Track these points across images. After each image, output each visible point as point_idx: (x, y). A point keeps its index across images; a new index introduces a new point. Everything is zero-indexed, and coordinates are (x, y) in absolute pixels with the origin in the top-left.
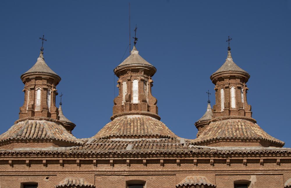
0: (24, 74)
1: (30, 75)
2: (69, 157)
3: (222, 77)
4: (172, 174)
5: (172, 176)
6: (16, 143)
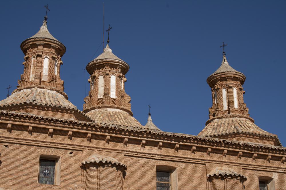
0: (30, 39)
1: (38, 41)
2: (99, 131)
3: (225, 77)
4: (202, 163)
5: (202, 165)
6: (32, 110)
